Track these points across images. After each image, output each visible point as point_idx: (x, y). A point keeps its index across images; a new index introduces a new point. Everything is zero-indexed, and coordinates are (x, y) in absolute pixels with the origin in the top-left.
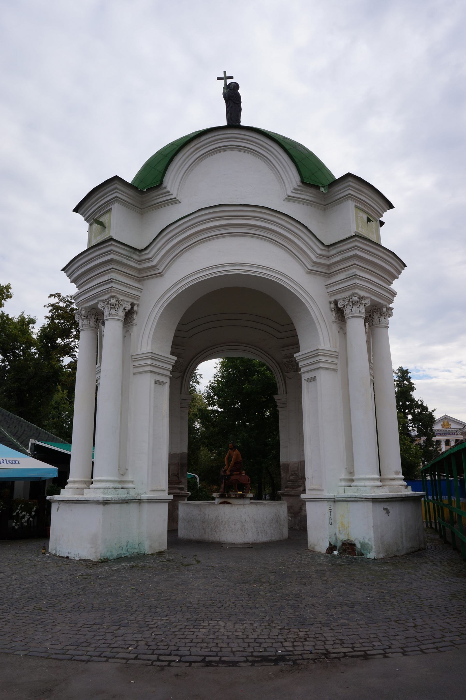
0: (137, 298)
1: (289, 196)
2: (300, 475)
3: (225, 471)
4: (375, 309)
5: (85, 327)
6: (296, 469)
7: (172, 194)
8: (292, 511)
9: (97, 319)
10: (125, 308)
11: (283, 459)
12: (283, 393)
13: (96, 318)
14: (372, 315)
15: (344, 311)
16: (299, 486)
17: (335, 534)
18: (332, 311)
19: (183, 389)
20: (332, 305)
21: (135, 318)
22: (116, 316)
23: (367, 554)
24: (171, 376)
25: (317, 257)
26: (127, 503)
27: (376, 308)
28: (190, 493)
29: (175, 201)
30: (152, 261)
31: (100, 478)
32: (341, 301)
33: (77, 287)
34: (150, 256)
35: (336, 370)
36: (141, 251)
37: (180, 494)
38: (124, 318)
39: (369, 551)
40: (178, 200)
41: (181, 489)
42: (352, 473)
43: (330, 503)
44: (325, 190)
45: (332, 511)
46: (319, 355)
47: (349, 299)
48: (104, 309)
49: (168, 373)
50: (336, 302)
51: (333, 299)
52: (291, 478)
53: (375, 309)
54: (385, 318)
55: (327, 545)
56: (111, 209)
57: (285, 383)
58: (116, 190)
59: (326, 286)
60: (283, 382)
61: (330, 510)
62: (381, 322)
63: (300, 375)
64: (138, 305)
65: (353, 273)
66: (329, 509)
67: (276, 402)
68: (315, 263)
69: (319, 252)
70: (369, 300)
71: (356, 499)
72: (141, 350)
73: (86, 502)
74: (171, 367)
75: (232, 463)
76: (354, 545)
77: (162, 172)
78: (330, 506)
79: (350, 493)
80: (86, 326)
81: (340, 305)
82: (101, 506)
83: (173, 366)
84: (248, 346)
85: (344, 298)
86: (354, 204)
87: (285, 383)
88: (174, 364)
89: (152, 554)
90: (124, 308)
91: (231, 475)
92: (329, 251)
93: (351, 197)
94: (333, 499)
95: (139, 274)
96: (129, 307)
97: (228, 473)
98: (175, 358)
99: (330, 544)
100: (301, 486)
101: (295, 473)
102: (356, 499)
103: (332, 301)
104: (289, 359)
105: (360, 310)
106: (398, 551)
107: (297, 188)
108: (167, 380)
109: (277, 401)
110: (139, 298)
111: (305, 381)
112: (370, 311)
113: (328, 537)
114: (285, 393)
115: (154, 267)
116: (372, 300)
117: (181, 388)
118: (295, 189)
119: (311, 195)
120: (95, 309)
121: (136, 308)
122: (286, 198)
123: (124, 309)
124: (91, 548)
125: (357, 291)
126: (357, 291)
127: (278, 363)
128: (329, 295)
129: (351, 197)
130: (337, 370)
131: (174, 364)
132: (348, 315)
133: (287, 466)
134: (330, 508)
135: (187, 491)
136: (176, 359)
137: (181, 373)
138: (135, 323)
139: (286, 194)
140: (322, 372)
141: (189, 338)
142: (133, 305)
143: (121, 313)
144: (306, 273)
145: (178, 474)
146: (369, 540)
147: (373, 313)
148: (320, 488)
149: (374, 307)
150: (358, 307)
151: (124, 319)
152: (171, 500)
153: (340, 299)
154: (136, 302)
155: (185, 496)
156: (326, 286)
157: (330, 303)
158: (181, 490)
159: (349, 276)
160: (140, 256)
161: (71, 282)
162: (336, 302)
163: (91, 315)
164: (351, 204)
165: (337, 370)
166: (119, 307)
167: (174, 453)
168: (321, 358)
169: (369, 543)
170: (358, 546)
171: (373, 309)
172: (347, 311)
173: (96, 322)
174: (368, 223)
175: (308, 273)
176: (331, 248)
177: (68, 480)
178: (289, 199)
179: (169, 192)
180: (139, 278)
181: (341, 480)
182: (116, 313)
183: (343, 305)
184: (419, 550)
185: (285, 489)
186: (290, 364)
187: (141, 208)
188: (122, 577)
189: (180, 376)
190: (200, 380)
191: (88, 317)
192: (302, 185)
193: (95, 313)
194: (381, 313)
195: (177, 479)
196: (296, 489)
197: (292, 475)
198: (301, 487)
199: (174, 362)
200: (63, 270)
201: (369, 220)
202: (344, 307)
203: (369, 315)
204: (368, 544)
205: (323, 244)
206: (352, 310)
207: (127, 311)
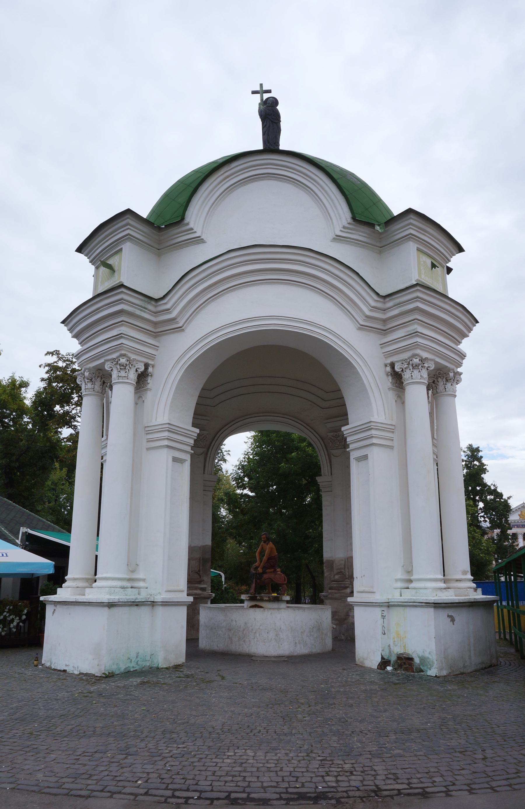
0: (152, 357)
1: (337, 236)
2: (347, 574)
3: (257, 568)
4: (439, 373)
5: (89, 391)
6: (343, 566)
7: (195, 232)
8: (337, 617)
9: (104, 382)
10: (138, 370)
11: (327, 555)
12: (327, 475)
13: (102, 381)
14: (436, 381)
15: (403, 376)
16: (346, 588)
17: (389, 646)
18: (388, 375)
19: (206, 469)
20: (389, 369)
21: (149, 381)
22: (126, 378)
23: (427, 671)
24: (193, 452)
25: (371, 310)
26: (137, 605)
27: (441, 372)
28: (214, 595)
29: (199, 240)
30: (170, 313)
31: (104, 575)
32: (400, 363)
33: (80, 344)
34: (168, 306)
35: (391, 447)
36: (157, 300)
37: (202, 596)
38: (135, 382)
39: (429, 666)
40: (202, 239)
41: (203, 589)
42: (410, 572)
43: (383, 609)
44: (380, 228)
45: (386, 617)
46: (372, 429)
47: (408, 362)
48: (112, 370)
49: (189, 449)
50: (392, 365)
51: (389, 361)
52: (337, 577)
53: (439, 373)
54: (452, 385)
55: (379, 660)
56: (122, 248)
57: (330, 462)
58: (128, 227)
59: (380, 345)
60: (328, 461)
61: (383, 617)
62: (447, 389)
63: (349, 453)
64: (153, 366)
65: (414, 330)
66: (382, 616)
67: (319, 485)
68: (367, 317)
69: (373, 304)
70: (433, 363)
71: (415, 604)
72: (156, 420)
73: (88, 603)
74: (192, 442)
75: (265, 558)
76: (412, 659)
77: (184, 204)
78: (383, 612)
79: (408, 596)
80: (90, 390)
81: (397, 369)
82: (106, 609)
83: (195, 440)
84: (286, 416)
85: (403, 360)
86: (416, 246)
87: (330, 462)
88: (196, 438)
89: (167, 668)
90: (136, 370)
91: (264, 573)
92: (385, 303)
93: (412, 238)
94: (387, 604)
95: (155, 328)
96: (142, 369)
97: (260, 570)
98: (197, 431)
99: (382, 658)
100: (348, 587)
101: (341, 572)
102: (415, 604)
103: (388, 364)
104: (336, 433)
105: (422, 375)
106: (464, 667)
107: (348, 226)
108: (188, 457)
109: (320, 484)
110: (155, 358)
111: (354, 460)
112: (434, 376)
113: (381, 649)
114: (330, 474)
115: (173, 320)
116: (436, 363)
117: (204, 467)
118: (344, 227)
119: (364, 235)
120: (100, 370)
121: (150, 369)
122: (334, 239)
123: (136, 371)
124: (93, 659)
125: (418, 351)
126: (418, 351)
127: (322, 438)
128: (384, 355)
129: (412, 238)
130: (393, 447)
131: (196, 438)
132: (407, 380)
133: (331, 563)
134: (383, 615)
135: (210, 591)
136: (198, 432)
137: (204, 449)
138: (149, 387)
139: (333, 234)
140: (375, 449)
141: (214, 406)
142: (147, 366)
143: (133, 376)
144: (357, 329)
145: (199, 571)
146: (430, 653)
147: (437, 378)
148: (371, 590)
149: (439, 371)
150: (419, 372)
151: (137, 383)
152: (191, 603)
153: (398, 361)
154: (150, 362)
155: (208, 598)
156: (380, 345)
157: (386, 366)
158: (203, 591)
159: (409, 333)
160: (156, 306)
161: (73, 337)
162: (392, 365)
163: (96, 377)
164: (412, 247)
165: (393, 447)
166: (130, 368)
167: (195, 545)
168: (373, 432)
169: (430, 657)
170: (417, 660)
171: (437, 374)
172: (406, 375)
173: (102, 386)
174: (432, 269)
175: (359, 329)
176: (388, 299)
177: (66, 577)
178: (338, 239)
179: (192, 229)
180: (155, 333)
181: (396, 580)
182: (127, 375)
183: (401, 368)
184: (490, 666)
185: (329, 591)
186: (336, 440)
187: (159, 248)
188: (130, 695)
189: (203, 453)
190: (227, 457)
191: (93, 380)
192: (353, 222)
193: (101, 375)
194: (448, 379)
195: (199, 577)
196: (343, 591)
197: (338, 574)
198: (349, 588)
199: (196, 435)
200: (63, 322)
201: (433, 266)
202: (402, 371)
203: (432, 381)
204: (428, 658)
205: (377, 294)
206: (412, 375)
207: (140, 373)
